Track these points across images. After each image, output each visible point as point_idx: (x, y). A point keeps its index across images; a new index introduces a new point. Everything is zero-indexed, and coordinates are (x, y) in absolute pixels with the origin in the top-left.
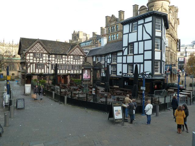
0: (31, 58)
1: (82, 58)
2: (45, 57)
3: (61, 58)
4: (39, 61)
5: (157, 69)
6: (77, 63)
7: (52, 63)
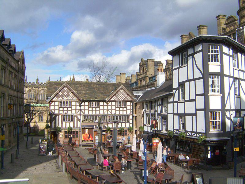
0: (57, 108)
1: (129, 105)
2: (75, 105)
3: (98, 106)
4: (66, 112)
6: (125, 112)
7: (84, 113)
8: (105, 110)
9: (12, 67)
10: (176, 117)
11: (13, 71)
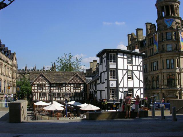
0: (36, 88)
4: (42, 90)
7: (53, 91)
9: (9, 64)
10: (100, 92)
11: (10, 66)
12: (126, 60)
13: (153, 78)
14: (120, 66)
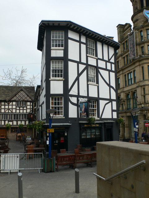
3: (25, 105)
5: (93, 112)
6: (21, 111)
8: (6, 109)
12: (83, 47)
13: (128, 94)
14: (73, 54)
